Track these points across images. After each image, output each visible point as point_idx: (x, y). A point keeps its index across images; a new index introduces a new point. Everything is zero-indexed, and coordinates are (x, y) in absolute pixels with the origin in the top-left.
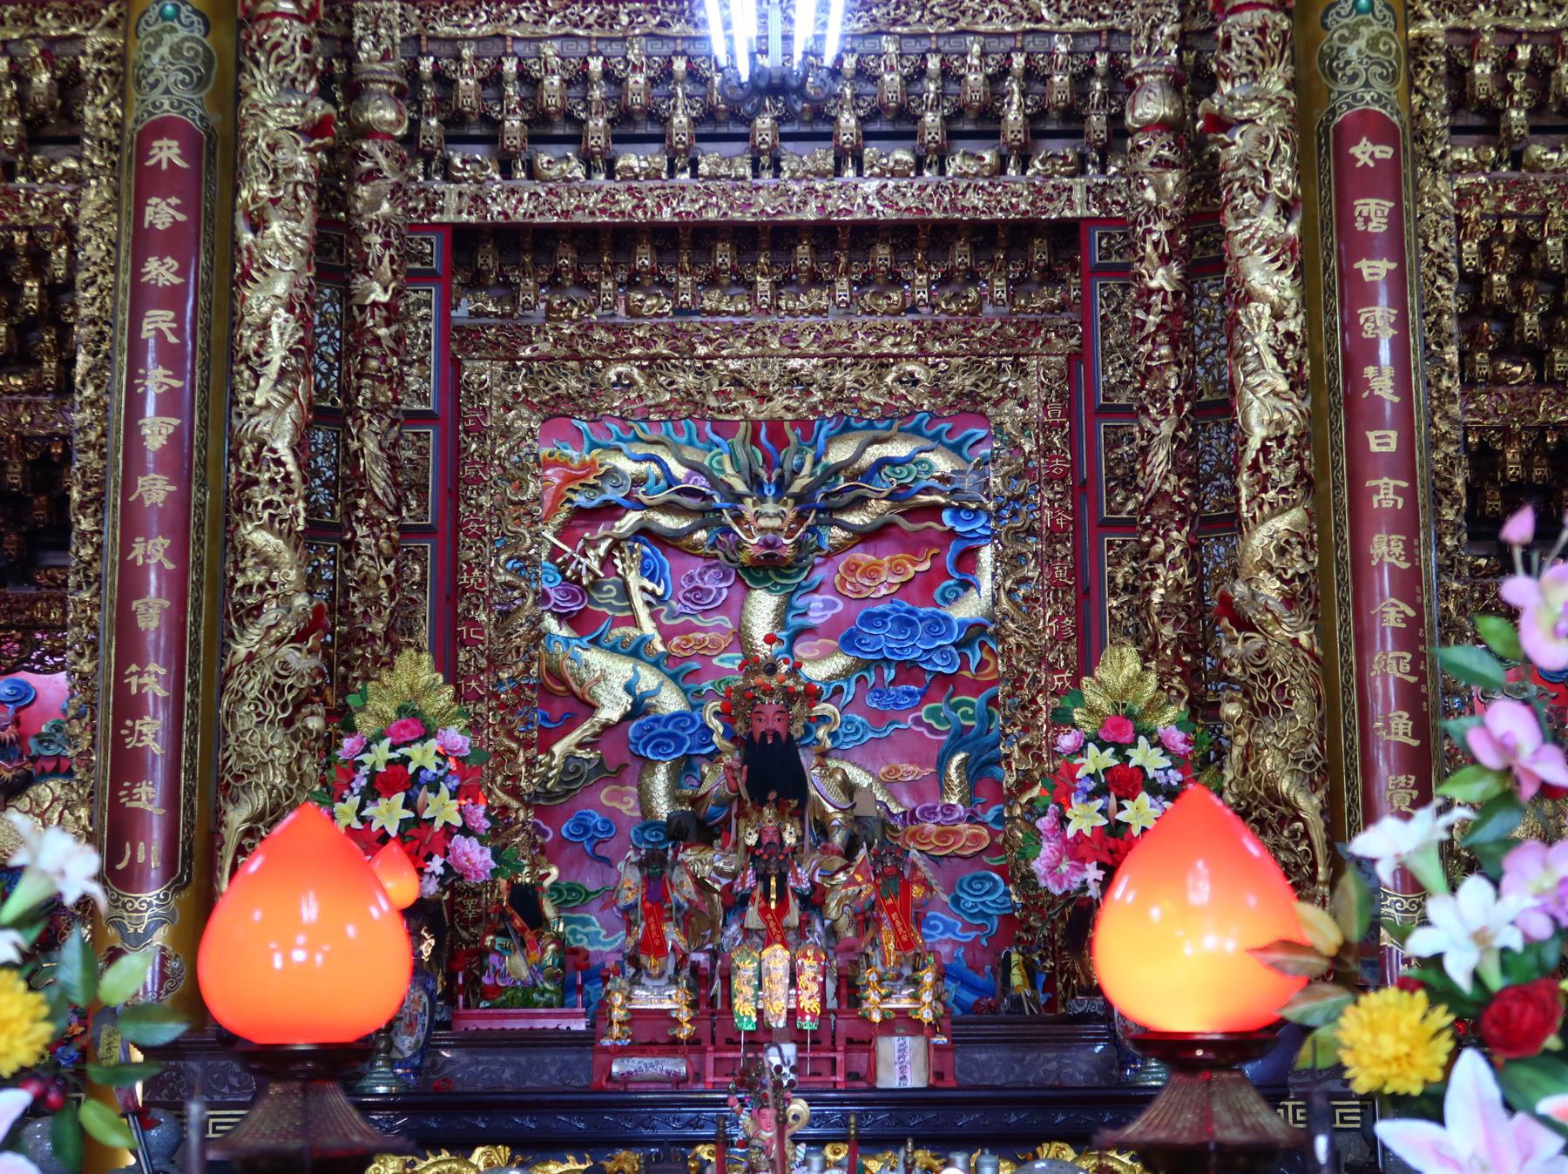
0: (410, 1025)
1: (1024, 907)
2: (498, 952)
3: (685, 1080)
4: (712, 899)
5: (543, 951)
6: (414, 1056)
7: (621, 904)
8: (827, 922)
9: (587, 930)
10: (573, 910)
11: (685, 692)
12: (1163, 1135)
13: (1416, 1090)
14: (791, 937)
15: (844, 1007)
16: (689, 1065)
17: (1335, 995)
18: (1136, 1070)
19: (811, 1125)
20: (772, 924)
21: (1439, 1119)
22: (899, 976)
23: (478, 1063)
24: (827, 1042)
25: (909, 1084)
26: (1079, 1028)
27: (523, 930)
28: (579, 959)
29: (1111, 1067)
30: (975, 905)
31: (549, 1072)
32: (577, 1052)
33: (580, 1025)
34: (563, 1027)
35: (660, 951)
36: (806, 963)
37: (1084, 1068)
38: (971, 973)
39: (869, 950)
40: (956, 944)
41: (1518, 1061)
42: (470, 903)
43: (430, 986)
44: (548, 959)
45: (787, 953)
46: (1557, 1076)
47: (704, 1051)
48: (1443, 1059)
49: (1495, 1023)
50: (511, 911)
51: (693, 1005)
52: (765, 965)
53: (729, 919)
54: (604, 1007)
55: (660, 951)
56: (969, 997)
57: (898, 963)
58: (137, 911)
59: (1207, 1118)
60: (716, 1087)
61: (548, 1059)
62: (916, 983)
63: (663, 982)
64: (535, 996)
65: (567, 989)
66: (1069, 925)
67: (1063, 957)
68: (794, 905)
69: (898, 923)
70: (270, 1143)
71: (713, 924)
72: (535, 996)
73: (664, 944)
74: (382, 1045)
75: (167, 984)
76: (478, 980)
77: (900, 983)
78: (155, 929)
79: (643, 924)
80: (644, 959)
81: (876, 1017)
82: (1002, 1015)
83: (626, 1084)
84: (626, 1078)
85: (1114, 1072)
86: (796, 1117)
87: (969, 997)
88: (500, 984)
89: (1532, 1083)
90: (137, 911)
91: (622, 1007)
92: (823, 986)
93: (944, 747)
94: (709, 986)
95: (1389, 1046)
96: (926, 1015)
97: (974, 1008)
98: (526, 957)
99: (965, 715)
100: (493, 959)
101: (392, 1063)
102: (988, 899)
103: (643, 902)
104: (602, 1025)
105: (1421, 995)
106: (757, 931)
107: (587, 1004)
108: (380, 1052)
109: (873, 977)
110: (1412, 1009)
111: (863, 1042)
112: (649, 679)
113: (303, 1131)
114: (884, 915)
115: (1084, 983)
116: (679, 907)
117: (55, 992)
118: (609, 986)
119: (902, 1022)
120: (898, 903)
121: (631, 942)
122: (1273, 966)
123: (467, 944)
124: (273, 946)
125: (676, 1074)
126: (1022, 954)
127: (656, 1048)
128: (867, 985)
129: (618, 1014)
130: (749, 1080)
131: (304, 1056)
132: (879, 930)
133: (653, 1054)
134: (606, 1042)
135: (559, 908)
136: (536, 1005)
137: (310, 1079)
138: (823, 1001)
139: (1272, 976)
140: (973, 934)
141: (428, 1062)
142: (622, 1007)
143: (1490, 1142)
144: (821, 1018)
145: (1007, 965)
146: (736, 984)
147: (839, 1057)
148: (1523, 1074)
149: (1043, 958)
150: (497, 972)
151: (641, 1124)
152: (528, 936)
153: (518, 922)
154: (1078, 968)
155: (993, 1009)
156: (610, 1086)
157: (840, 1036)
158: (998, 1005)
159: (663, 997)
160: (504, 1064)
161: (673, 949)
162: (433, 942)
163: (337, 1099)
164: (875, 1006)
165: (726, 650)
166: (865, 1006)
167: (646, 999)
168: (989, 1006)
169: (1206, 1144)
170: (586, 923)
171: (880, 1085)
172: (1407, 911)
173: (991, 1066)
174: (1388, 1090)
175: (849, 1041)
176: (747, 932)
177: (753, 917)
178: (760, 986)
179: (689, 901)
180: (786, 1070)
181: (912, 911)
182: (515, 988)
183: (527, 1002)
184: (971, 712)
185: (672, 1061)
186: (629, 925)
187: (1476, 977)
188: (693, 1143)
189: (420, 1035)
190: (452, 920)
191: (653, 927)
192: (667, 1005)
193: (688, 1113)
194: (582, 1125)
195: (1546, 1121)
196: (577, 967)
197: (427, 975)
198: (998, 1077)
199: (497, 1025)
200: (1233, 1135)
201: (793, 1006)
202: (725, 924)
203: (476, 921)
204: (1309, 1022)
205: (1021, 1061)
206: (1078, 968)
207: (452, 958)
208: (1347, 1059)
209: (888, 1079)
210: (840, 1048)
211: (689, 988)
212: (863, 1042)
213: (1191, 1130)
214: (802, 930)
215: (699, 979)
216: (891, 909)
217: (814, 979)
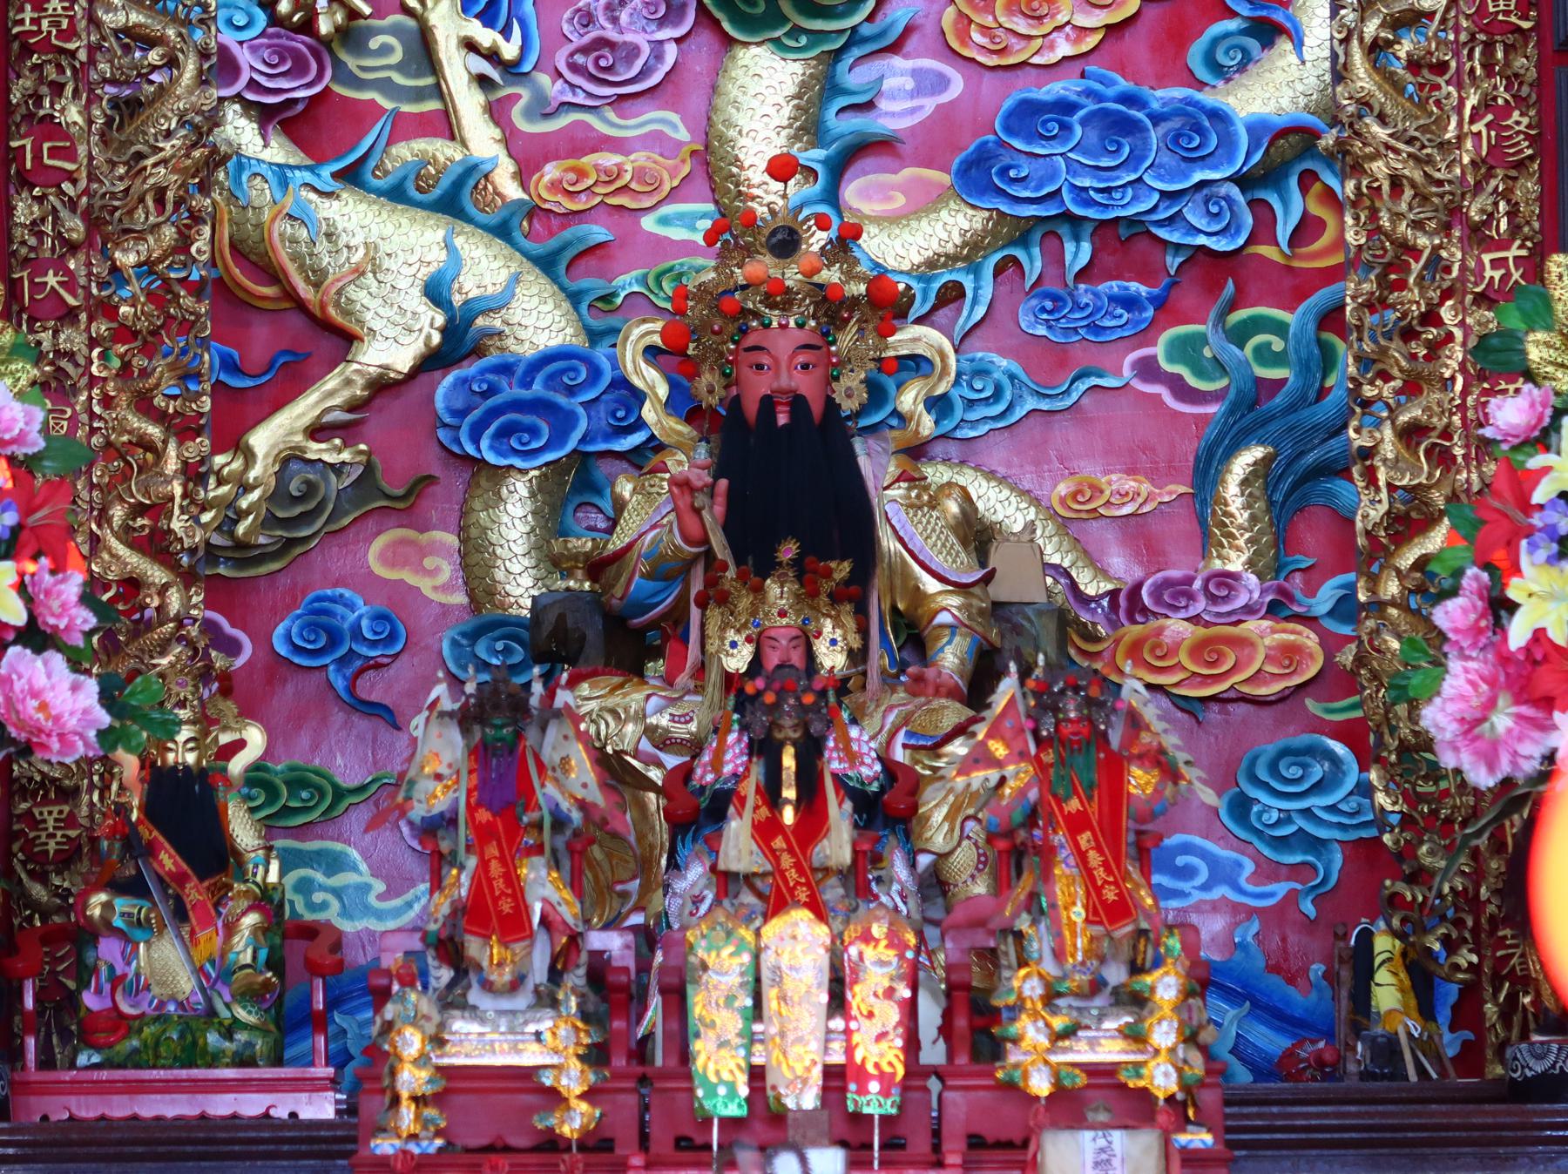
1: (1407, 821)
4: (642, 807)
5: (231, 929)
7: (418, 812)
8: (924, 860)
10: (301, 832)
11: (574, 298)
14: (833, 892)
15: (962, 1060)
20: (787, 861)
22: (1097, 985)
24: (920, 1144)
27: (181, 879)
28: (318, 951)
30: (1285, 819)
33: (321, 1108)
34: (281, 1113)
35: (514, 926)
36: (870, 953)
38: (1276, 981)
39: (1023, 923)
42: (50, 815)
44: (243, 949)
45: (822, 931)
50: (148, 833)
51: (595, 1056)
52: (768, 959)
53: (683, 852)
55: (514, 926)
56: (1270, 1041)
62: (1138, 1001)
63: (522, 1000)
64: (213, 1038)
65: (290, 1022)
68: (839, 814)
69: (1094, 858)
71: (645, 866)
72: (213, 1038)
76: (73, 999)
77: (1099, 1001)
79: (472, 862)
80: (474, 947)
81: (1040, 1085)
82: (1352, 1082)
87: (1270, 1041)
91: (421, 1060)
92: (910, 1010)
93: (1211, 432)
96: (1162, 1080)
97: (1283, 1067)
99: (1263, 354)
100: (109, 950)
102: (1316, 802)
104: (372, 1105)
106: (749, 879)
107: (340, 1059)
109: (1033, 989)
112: (484, 268)
114: (1059, 838)
116: (559, 822)
118: (390, 1011)
120: (1093, 810)
126: (1399, 935)
128: (1017, 1009)
129: (412, 1079)
132: (1046, 875)
135: (269, 828)
136: (213, 1060)
138: (912, 1044)
140: (1281, 889)
142: (421, 1060)
144: (905, 1087)
145: (1362, 964)
146: (698, 1005)
149: (1450, 945)
150: (116, 981)
152: (194, 893)
153: (168, 860)
155: (1327, 1068)
158: (1340, 1060)
164: (1036, 1057)
165: (673, 195)
166: (1014, 1056)
167: (485, 1040)
168: (1320, 1063)
170: (334, 864)
175: (976, 1142)
176: (726, 882)
177: (739, 844)
178: (757, 1011)
179: (582, 805)
182: (161, 1018)
183: (194, 1054)
184: (1278, 345)
186: (438, 866)
191: (495, 868)
192: (531, 1056)
196: (314, 969)
199: (119, 1107)
201: (838, 1058)
203: (66, 859)
211: (585, 1016)
212: (1008, 1145)
214: (860, 878)
216: (1076, 824)
217: (890, 993)
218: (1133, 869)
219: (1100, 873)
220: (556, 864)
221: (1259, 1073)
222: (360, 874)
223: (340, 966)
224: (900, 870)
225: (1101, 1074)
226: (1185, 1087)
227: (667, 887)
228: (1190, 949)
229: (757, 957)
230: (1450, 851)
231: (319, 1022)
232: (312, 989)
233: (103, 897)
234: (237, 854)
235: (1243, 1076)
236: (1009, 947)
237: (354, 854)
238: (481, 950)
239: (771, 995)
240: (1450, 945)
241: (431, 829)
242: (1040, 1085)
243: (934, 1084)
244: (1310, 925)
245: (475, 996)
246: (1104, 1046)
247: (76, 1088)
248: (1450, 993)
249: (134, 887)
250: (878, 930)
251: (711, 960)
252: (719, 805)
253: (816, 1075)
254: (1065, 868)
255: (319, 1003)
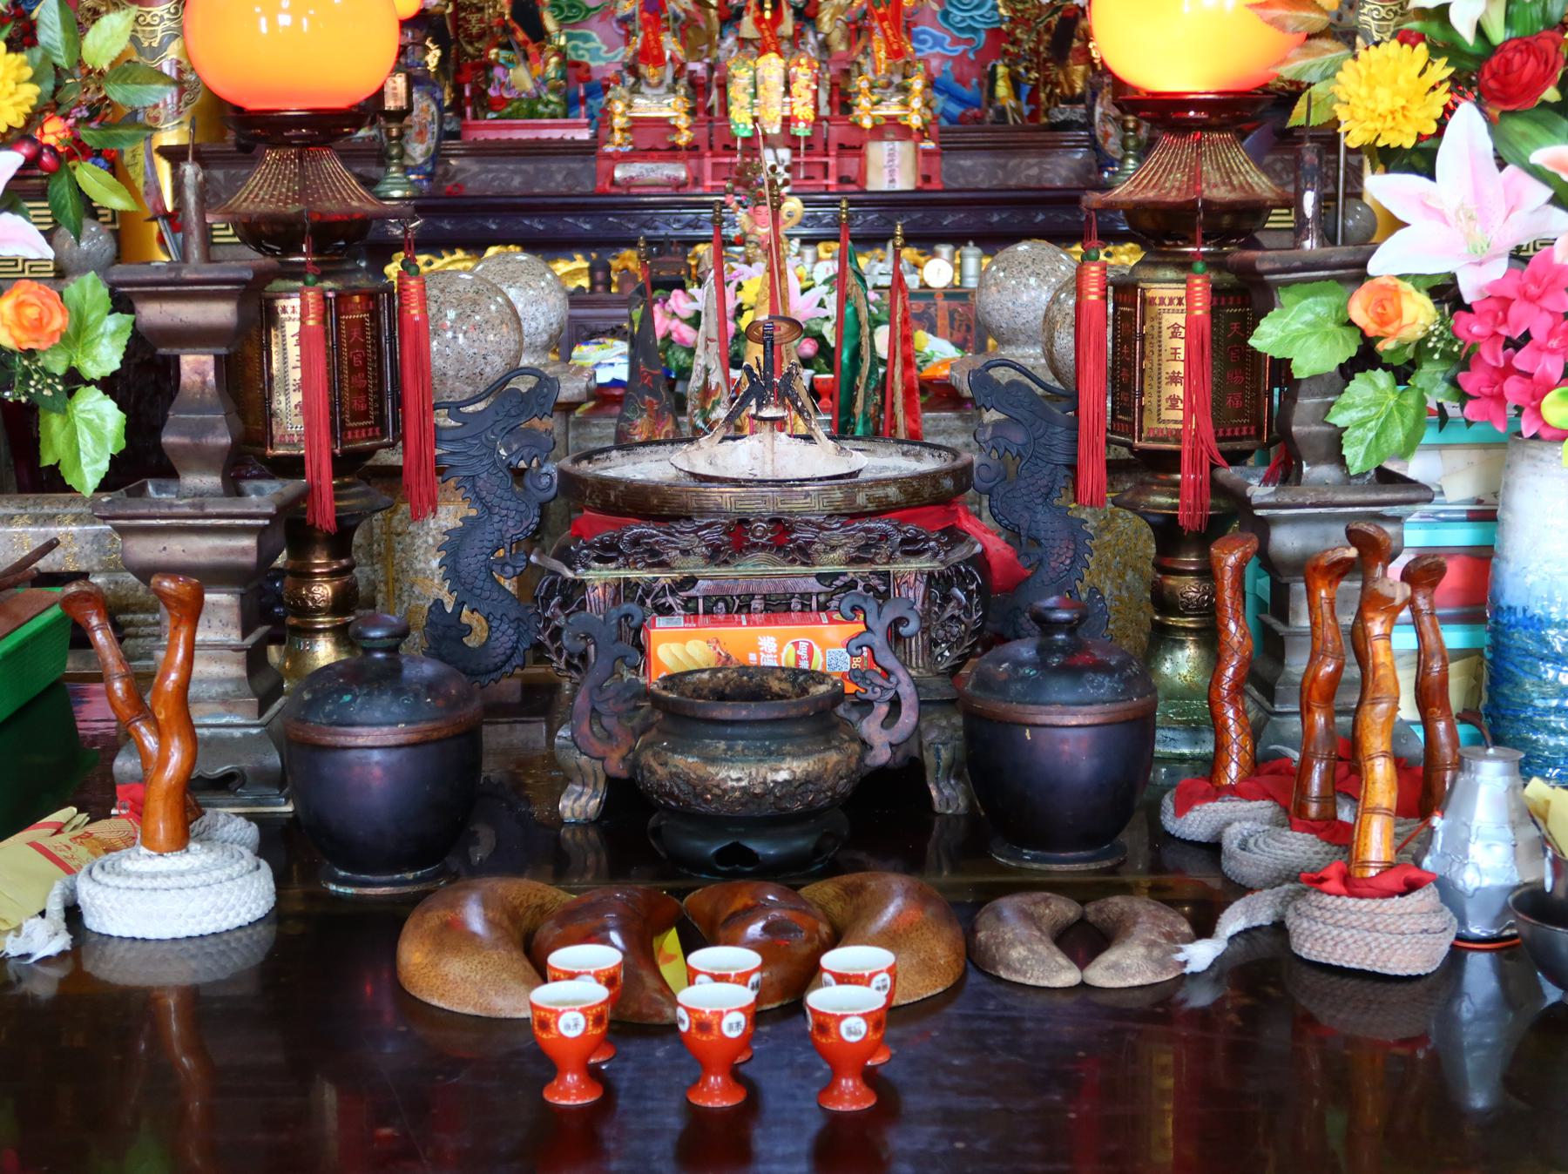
0: (420, 133)
1: (1012, 20)
2: (502, 65)
3: (684, 185)
4: (708, 15)
5: (546, 63)
6: (426, 163)
7: (620, 14)
8: (820, 36)
9: (588, 46)
10: (574, 26)
12: (1151, 195)
13: (1409, 143)
14: (785, 46)
15: (836, 114)
16: (689, 169)
17: (1331, 50)
18: (1113, 173)
19: (801, 224)
20: (767, 33)
21: (1431, 175)
22: (890, 84)
23: (489, 171)
24: (819, 148)
25: (898, 186)
26: (1060, 135)
27: (526, 43)
28: (581, 72)
29: (1089, 171)
30: (963, 20)
31: (556, 178)
32: (584, 161)
33: (584, 135)
34: (568, 137)
35: (658, 60)
36: (800, 71)
37: (1064, 173)
38: (958, 86)
39: (861, 59)
40: (945, 58)
41: (1513, 113)
42: (474, 18)
43: (438, 95)
44: (551, 71)
45: (782, 62)
46: (1551, 130)
47: (701, 156)
48: (1439, 112)
49: (1494, 75)
50: (513, 25)
51: (692, 112)
52: (760, 73)
53: (725, 32)
54: (607, 114)
55: (658, 60)
56: (955, 110)
57: (890, 72)
58: (149, 25)
59: (1196, 177)
60: (714, 191)
61: (554, 167)
62: (905, 90)
63: (662, 90)
64: (540, 108)
65: (571, 103)
66: (1055, 36)
67: (1047, 69)
68: (788, 14)
69: (889, 32)
70: (263, 208)
71: (710, 39)
72: (540, 108)
73: (662, 54)
74: (394, 152)
75: (186, 97)
76: (485, 93)
77: (891, 90)
78: (169, 43)
79: (641, 34)
80: (643, 69)
81: (867, 123)
82: (988, 125)
83: (629, 188)
84: (629, 183)
85: (1092, 177)
86: (790, 215)
87: (955, 110)
88: (506, 95)
89: (1524, 136)
90: (149, 25)
91: (623, 114)
92: (816, 93)
94: (706, 93)
95: (1385, 100)
96: (915, 121)
97: (961, 120)
98: (530, 70)
100: (498, 72)
101: (406, 170)
102: (975, 13)
103: (641, 12)
104: (604, 133)
105: (1422, 47)
106: (751, 41)
107: (591, 117)
108: (391, 158)
109: (864, 85)
110: (1412, 62)
111: (854, 149)
113: (302, 195)
114: (875, 24)
115: (1067, 91)
116: (676, 18)
117: (37, 53)
118: (610, 94)
119: (893, 128)
120: (889, 12)
121: (630, 52)
122: (1272, 22)
123: (473, 58)
124: (258, 10)
125: (676, 179)
126: (1007, 66)
127: (655, 154)
128: (858, 93)
129: (619, 122)
130: (745, 180)
131: (297, 122)
132: (870, 39)
133: (653, 160)
134: (609, 149)
135: (562, 25)
136: (541, 116)
137: (305, 146)
138: (817, 108)
139: (1271, 31)
140: (961, 48)
141: (440, 170)
142: (623, 114)
143: (1478, 194)
144: (814, 125)
145: (992, 78)
146: (732, 92)
147: (831, 161)
148: (1517, 126)
149: (1028, 70)
150: (502, 84)
151: (645, 225)
152: (531, 49)
153: (521, 36)
154: (1062, 77)
155: (978, 120)
156: (614, 190)
157: (832, 142)
158: (983, 117)
159: (663, 105)
160: (514, 172)
161: (672, 59)
162: (438, 53)
163: (332, 165)
164: (866, 112)
166: (857, 112)
167: (649, 106)
168: (975, 117)
169: (1195, 201)
170: (587, 39)
171: (870, 188)
172: (1384, 19)
173: (975, 171)
174: (1380, 144)
175: (841, 146)
176: (743, 42)
177: (748, 27)
178: (755, 95)
179: (685, 11)
180: (780, 169)
181: (903, 18)
182: (520, 99)
183: (533, 114)
185: (672, 166)
186: (627, 38)
187: (1480, 31)
188: (694, 242)
189: (430, 142)
190: (457, 35)
191: (651, 37)
192: (666, 113)
193: (689, 215)
194: (587, 227)
195: (1537, 173)
196: (580, 80)
197: (434, 85)
198: (982, 180)
199: (505, 135)
200: (1221, 194)
201: (787, 113)
202: (722, 38)
203: (480, 36)
204: (1305, 79)
205: (1003, 167)
206: (1062, 77)
207: (459, 71)
208: (1342, 114)
209: (878, 181)
210: (833, 153)
211: (687, 96)
212: (854, 148)
213: (1179, 189)
214: (797, 39)
215: (698, 88)
216: (882, 18)
217: (808, 87)
218: (904, 36)
219: (892, 39)
220: (675, 35)
221: (951, 121)
222: (597, 42)
223: (589, 79)
224: (811, 39)
225: (891, 119)
226: (924, 124)
227: (718, 46)
228: (927, 69)
229: (755, 71)
230: (1029, 31)
231: (582, 101)
232: (581, 89)
233: (494, 51)
234: (548, 33)
235: (944, 123)
236: (855, 68)
237: (594, 35)
238: (647, 70)
239: (761, 91)
240: (1028, 70)
241: (624, 21)
242: (867, 123)
243: (825, 123)
244: (971, 63)
245: (643, 89)
246: (892, 108)
247: (487, 127)
248: (1026, 89)
249: (507, 46)
250: (803, 61)
251: (737, 73)
252: (738, 14)
253: (779, 120)
254: (878, 36)
255: (582, 93)
